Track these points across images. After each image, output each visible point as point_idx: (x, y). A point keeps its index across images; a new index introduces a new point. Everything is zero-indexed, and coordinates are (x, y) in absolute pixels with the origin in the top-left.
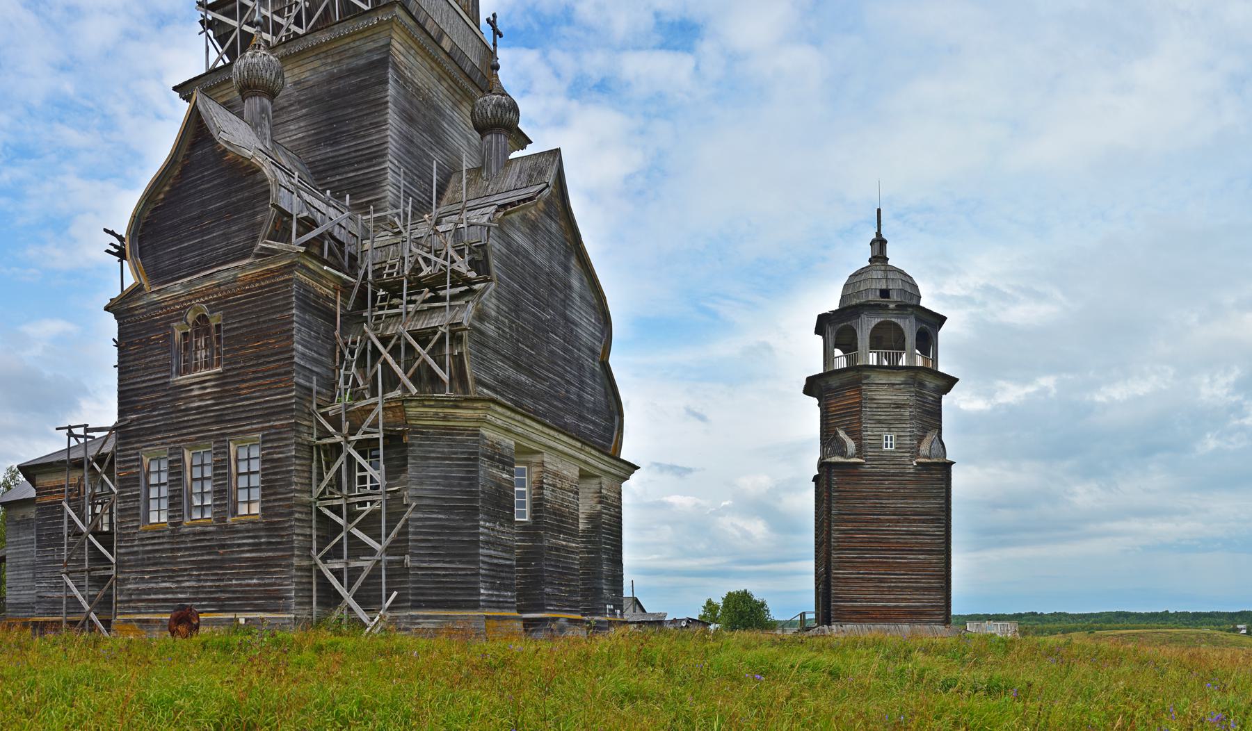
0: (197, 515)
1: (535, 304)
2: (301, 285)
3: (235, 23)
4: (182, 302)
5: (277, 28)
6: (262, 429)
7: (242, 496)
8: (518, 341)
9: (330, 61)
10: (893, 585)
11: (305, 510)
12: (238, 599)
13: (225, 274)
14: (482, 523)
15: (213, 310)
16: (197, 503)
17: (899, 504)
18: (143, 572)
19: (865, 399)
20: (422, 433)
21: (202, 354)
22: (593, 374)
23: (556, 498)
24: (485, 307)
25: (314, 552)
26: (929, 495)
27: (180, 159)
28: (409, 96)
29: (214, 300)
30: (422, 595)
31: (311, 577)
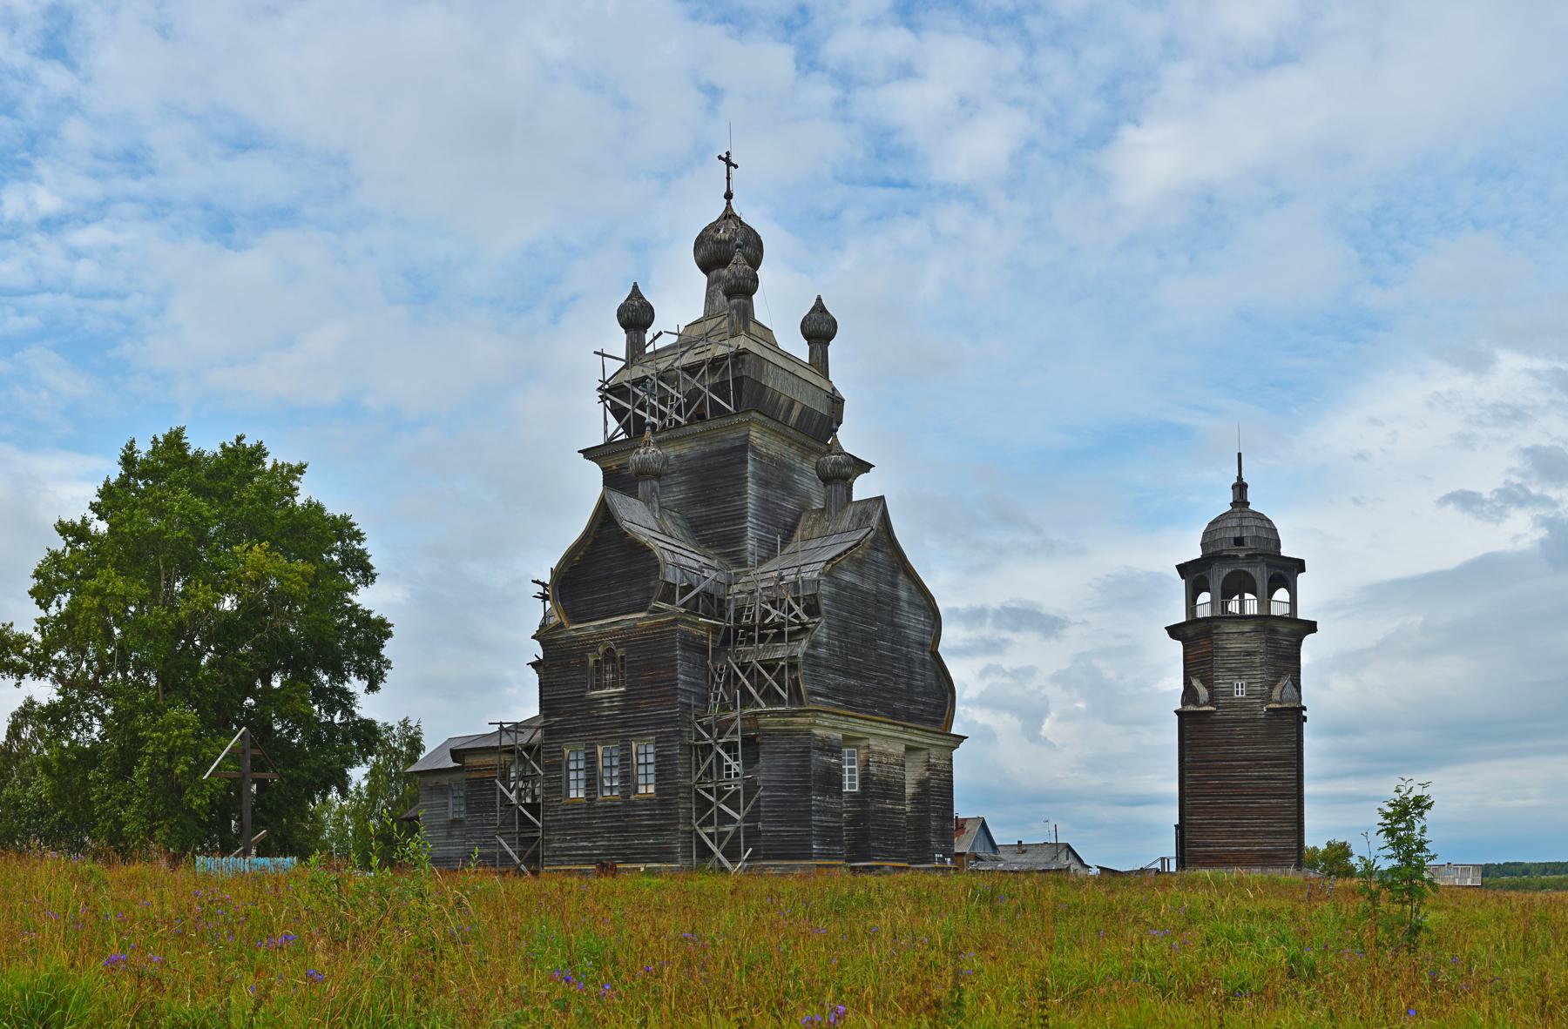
0: (607, 793)
1: (863, 623)
2: (682, 632)
3: (629, 407)
4: (595, 639)
5: (662, 415)
6: (656, 733)
7: (641, 780)
8: (847, 654)
9: (703, 443)
10: (1245, 829)
11: (687, 791)
12: (639, 854)
13: (627, 623)
14: (814, 797)
15: (619, 646)
16: (607, 784)
17: (1251, 750)
18: (565, 835)
19: (1216, 648)
20: (770, 735)
21: (609, 676)
22: (923, 663)
23: (882, 771)
24: (818, 638)
25: (694, 821)
26: (1280, 739)
27: (592, 533)
28: (765, 467)
29: (620, 639)
30: (771, 850)
31: (692, 838)
